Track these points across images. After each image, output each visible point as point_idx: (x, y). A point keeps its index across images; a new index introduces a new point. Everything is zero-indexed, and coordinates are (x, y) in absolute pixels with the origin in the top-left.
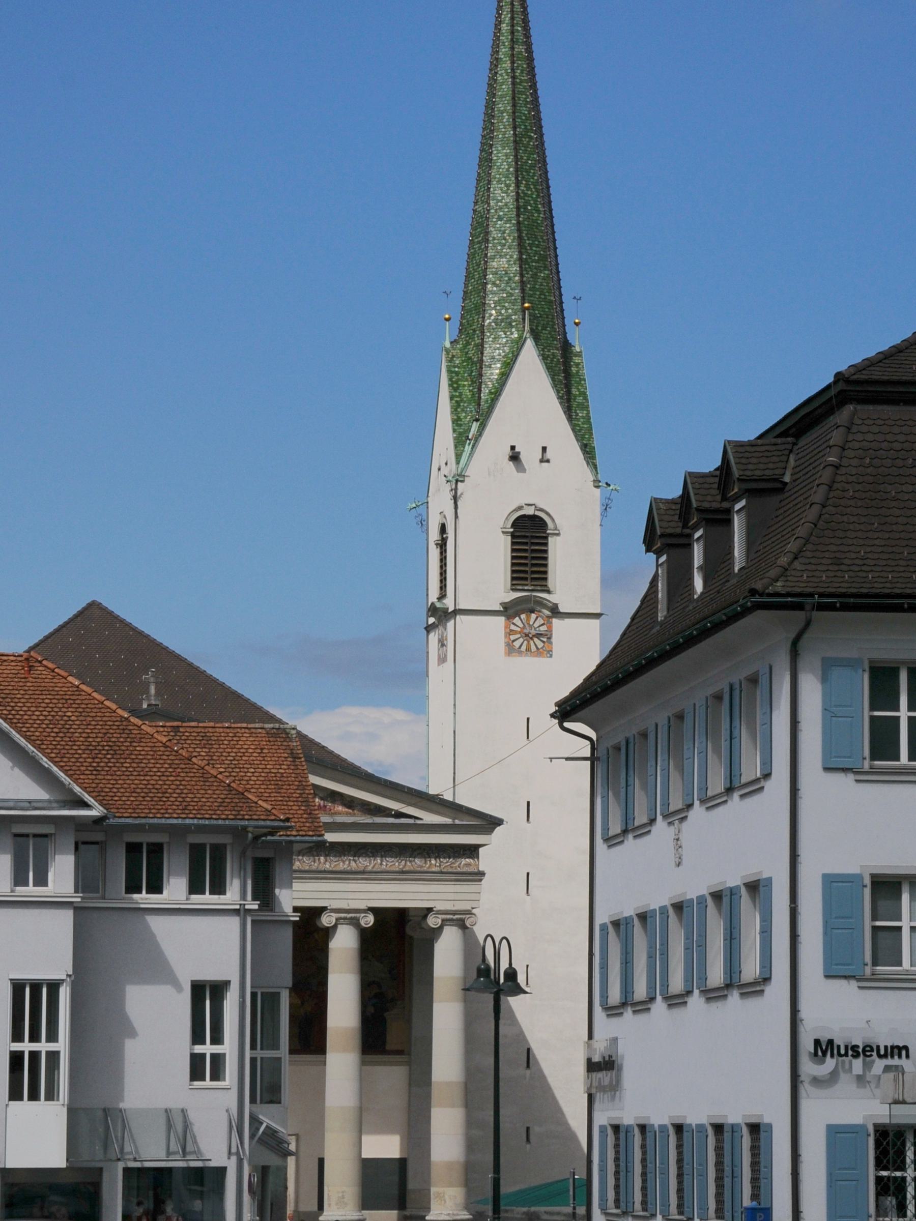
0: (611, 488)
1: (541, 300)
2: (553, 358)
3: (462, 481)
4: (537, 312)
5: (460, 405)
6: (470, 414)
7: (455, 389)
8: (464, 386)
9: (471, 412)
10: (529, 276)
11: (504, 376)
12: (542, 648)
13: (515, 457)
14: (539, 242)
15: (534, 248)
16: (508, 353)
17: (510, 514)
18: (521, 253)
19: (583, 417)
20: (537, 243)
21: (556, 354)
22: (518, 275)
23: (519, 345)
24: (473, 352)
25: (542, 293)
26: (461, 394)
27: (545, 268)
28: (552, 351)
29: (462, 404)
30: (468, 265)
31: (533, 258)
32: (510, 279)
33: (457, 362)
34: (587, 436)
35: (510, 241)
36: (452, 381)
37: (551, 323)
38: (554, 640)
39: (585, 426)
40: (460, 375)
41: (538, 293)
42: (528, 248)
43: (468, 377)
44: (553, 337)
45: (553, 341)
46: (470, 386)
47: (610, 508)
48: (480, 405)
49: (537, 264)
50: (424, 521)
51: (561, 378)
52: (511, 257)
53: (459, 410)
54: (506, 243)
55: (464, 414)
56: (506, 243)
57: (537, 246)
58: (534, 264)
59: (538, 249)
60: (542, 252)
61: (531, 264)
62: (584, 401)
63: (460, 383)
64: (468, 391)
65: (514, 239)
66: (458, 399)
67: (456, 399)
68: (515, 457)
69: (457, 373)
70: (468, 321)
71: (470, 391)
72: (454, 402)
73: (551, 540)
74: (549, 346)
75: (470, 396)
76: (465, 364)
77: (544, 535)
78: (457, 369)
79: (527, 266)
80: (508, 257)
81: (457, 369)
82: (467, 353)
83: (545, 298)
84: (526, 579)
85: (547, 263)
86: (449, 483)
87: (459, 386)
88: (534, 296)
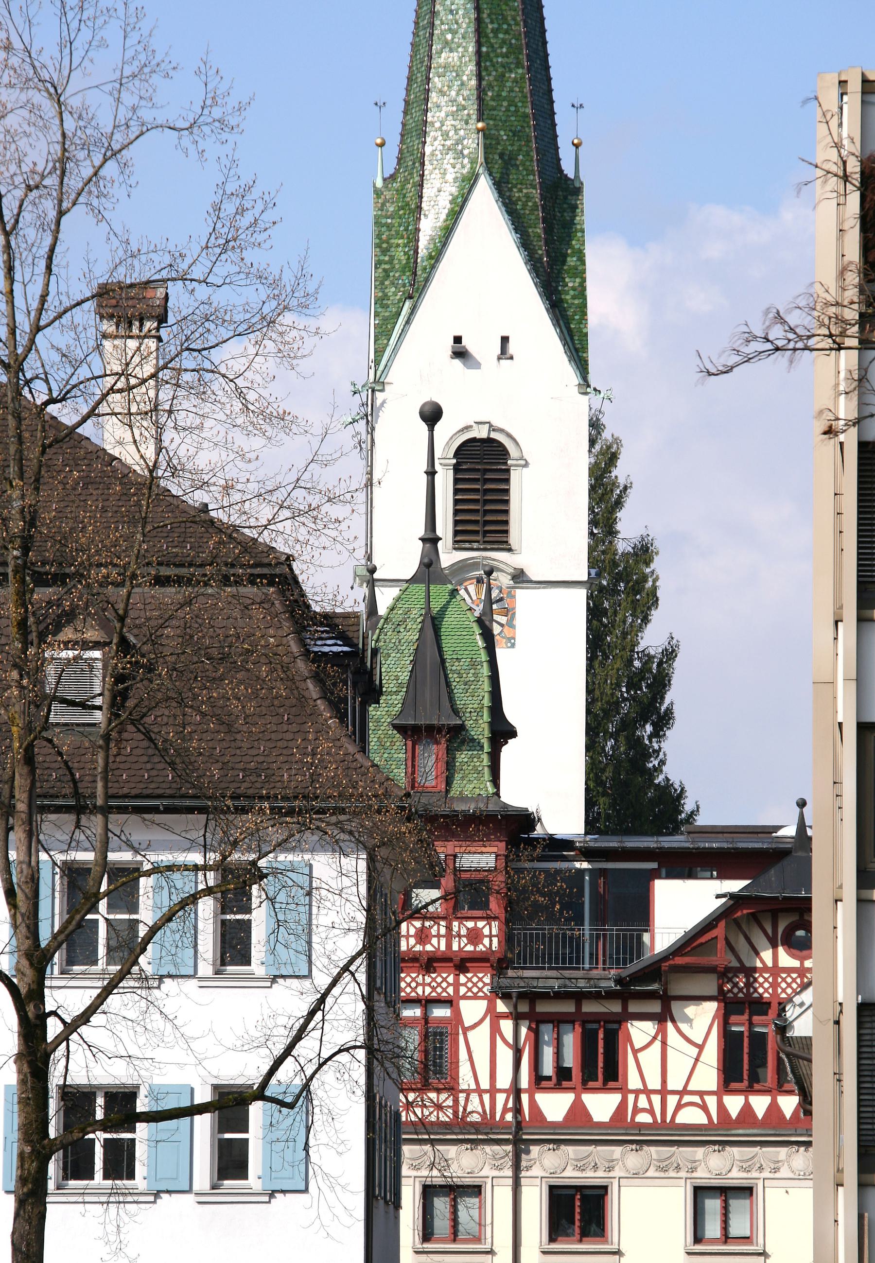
0: (602, 395)
1: (510, 114)
2: (527, 201)
3: (382, 390)
4: (502, 133)
5: (389, 276)
6: (402, 289)
7: (384, 252)
8: (398, 245)
9: (404, 286)
10: (491, 78)
11: (448, 232)
12: (499, 634)
13: (460, 353)
14: (509, 25)
15: (501, 36)
16: (457, 197)
17: (451, 438)
18: (479, 44)
19: (574, 289)
20: (505, 26)
21: (531, 195)
22: (474, 78)
23: (469, 183)
24: (411, 194)
25: (512, 103)
26: (392, 258)
27: (519, 65)
28: (525, 191)
29: (391, 274)
30: (411, 61)
31: (499, 51)
32: (463, 84)
33: (391, 209)
34: (577, 317)
35: (464, 25)
36: (380, 239)
37: (525, 149)
38: (518, 621)
39: (576, 302)
40: (394, 229)
41: (505, 104)
42: (491, 35)
43: (404, 233)
44: (527, 170)
45: (528, 175)
46: (405, 246)
47: (355, 447)
48: (416, 275)
49: (506, 60)
50: (364, 442)
51: (539, 231)
52: (466, 49)
53: (387, 283)
54: (458, 29)
55: (393, 289)
56: (458, 29)
57: (506, 32)
58: (500, 60)
59: (507, 36)
60: (513, 41)
61: (495, 60)
62: (578, 263)
63: (392, 241)
64: (402, 253)
65: (470, 23)
66: (387, 266)
67: (383, 266)
68: (460, 353)
69: (389, 227)
70: (407, 147)
71: (405, 253)
72: (380, 270)
73: (514, 475)
74: (521, 184)
75: (404, 262)
76: (401, 212)
77: (504, 467)
78: (389, 221)
79: (488, 64)
80: (460, 50)
81: (389, 221)
82: (404, 196)
83: (517, 111)
84: (476, 532)
85: (521, 56)
86: (357, 395)
87: (390, 246)
88: (498, 108)
